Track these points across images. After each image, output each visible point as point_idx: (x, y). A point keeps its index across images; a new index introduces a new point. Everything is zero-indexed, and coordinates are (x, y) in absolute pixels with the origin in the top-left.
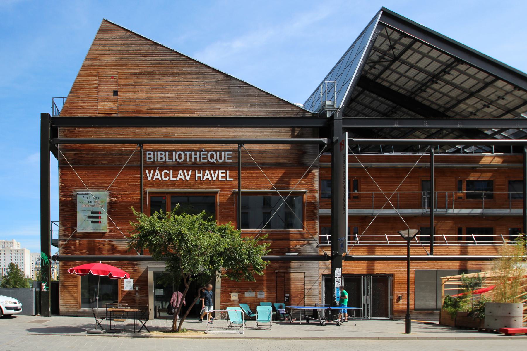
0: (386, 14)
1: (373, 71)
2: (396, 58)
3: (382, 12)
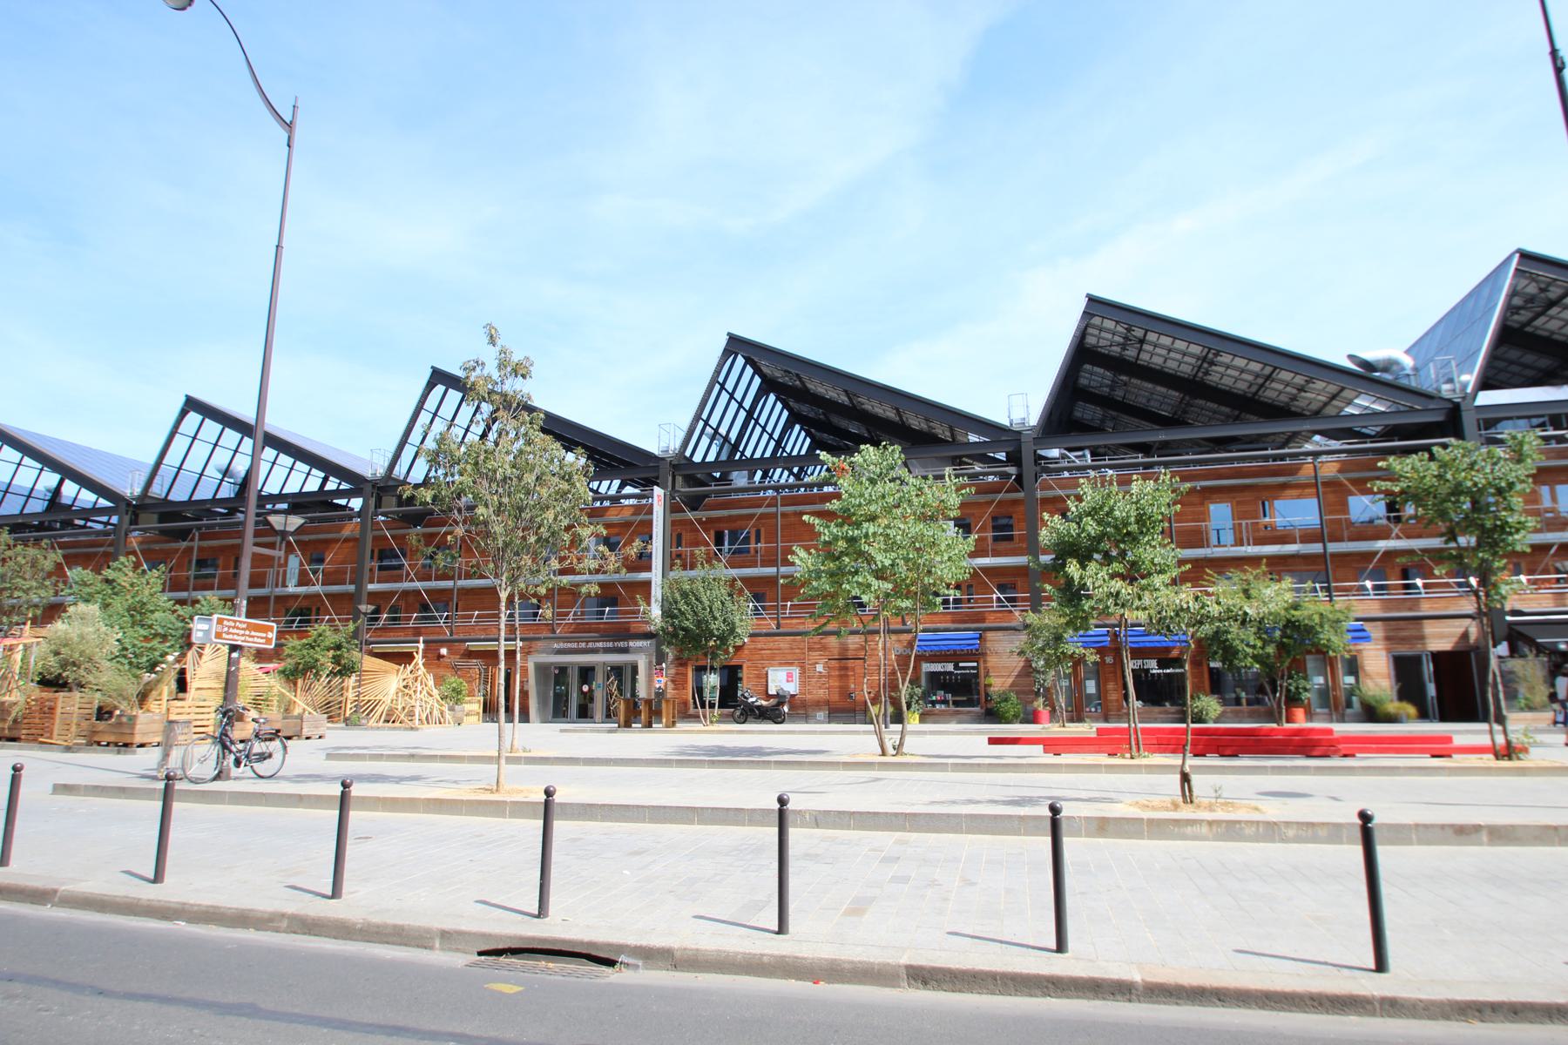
0: (1525, 256)
1: (1516, 317)
2: (1552, 304)
3: (1517, 255)
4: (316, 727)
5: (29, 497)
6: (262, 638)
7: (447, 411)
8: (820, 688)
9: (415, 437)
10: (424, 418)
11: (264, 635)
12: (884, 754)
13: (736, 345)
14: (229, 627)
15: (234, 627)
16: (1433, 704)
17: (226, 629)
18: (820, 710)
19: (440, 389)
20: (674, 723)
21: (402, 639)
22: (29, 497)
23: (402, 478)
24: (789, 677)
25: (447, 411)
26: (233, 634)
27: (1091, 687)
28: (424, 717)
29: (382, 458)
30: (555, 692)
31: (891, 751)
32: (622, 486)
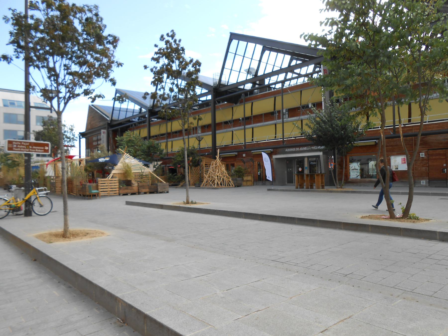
4: (164, 188)
5: (127, 111)
6: (41, 149)
7: (241, 51)
8: (423, 166)
9: (228, 65)
10: (231, 56)
11: (43, 148)
12: (392, 217)
13: (233, 36)
14: (17, 145)
15: (20, 145)
16: (336, 181)
17: (15, 146)
18: (423, 179)
19: (235, 42)
20: (323, 187)
21: (230, 151)
22: (120, 111)
23: (226, 84)
24: (403, 161)
25: (241, 51)
26: (21, 148)
27: (334, 109)
28: (219, 183)
29: (217, 76)
30: (287, 172)
31: (398, 213)
32: (315, 68)
